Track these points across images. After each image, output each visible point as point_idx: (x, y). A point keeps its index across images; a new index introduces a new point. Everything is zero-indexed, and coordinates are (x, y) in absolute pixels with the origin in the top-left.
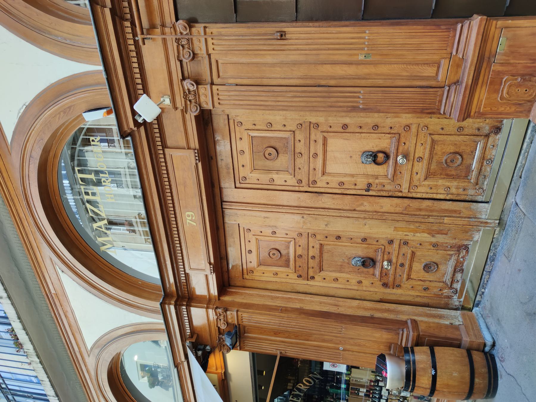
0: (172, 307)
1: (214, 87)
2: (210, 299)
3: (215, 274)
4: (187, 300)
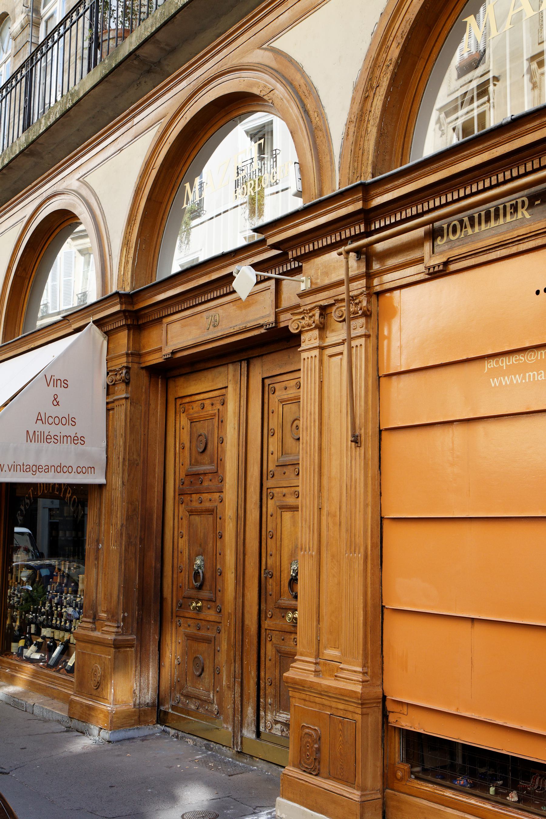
0: (117, 308)
1: (316, 352)
2: (142, 355)
3: (164, 360)
4: (135, 323)
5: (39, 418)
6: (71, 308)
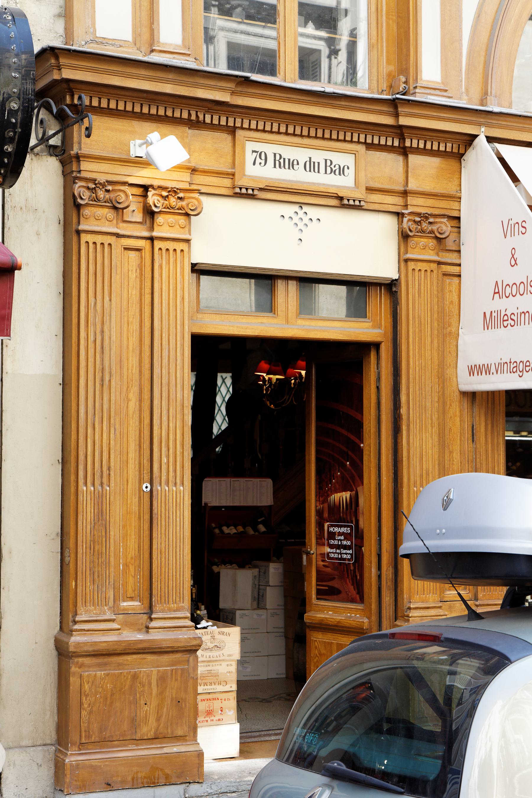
5: (497, 291)
6: (511, 98)
